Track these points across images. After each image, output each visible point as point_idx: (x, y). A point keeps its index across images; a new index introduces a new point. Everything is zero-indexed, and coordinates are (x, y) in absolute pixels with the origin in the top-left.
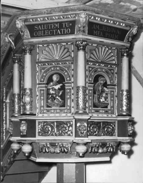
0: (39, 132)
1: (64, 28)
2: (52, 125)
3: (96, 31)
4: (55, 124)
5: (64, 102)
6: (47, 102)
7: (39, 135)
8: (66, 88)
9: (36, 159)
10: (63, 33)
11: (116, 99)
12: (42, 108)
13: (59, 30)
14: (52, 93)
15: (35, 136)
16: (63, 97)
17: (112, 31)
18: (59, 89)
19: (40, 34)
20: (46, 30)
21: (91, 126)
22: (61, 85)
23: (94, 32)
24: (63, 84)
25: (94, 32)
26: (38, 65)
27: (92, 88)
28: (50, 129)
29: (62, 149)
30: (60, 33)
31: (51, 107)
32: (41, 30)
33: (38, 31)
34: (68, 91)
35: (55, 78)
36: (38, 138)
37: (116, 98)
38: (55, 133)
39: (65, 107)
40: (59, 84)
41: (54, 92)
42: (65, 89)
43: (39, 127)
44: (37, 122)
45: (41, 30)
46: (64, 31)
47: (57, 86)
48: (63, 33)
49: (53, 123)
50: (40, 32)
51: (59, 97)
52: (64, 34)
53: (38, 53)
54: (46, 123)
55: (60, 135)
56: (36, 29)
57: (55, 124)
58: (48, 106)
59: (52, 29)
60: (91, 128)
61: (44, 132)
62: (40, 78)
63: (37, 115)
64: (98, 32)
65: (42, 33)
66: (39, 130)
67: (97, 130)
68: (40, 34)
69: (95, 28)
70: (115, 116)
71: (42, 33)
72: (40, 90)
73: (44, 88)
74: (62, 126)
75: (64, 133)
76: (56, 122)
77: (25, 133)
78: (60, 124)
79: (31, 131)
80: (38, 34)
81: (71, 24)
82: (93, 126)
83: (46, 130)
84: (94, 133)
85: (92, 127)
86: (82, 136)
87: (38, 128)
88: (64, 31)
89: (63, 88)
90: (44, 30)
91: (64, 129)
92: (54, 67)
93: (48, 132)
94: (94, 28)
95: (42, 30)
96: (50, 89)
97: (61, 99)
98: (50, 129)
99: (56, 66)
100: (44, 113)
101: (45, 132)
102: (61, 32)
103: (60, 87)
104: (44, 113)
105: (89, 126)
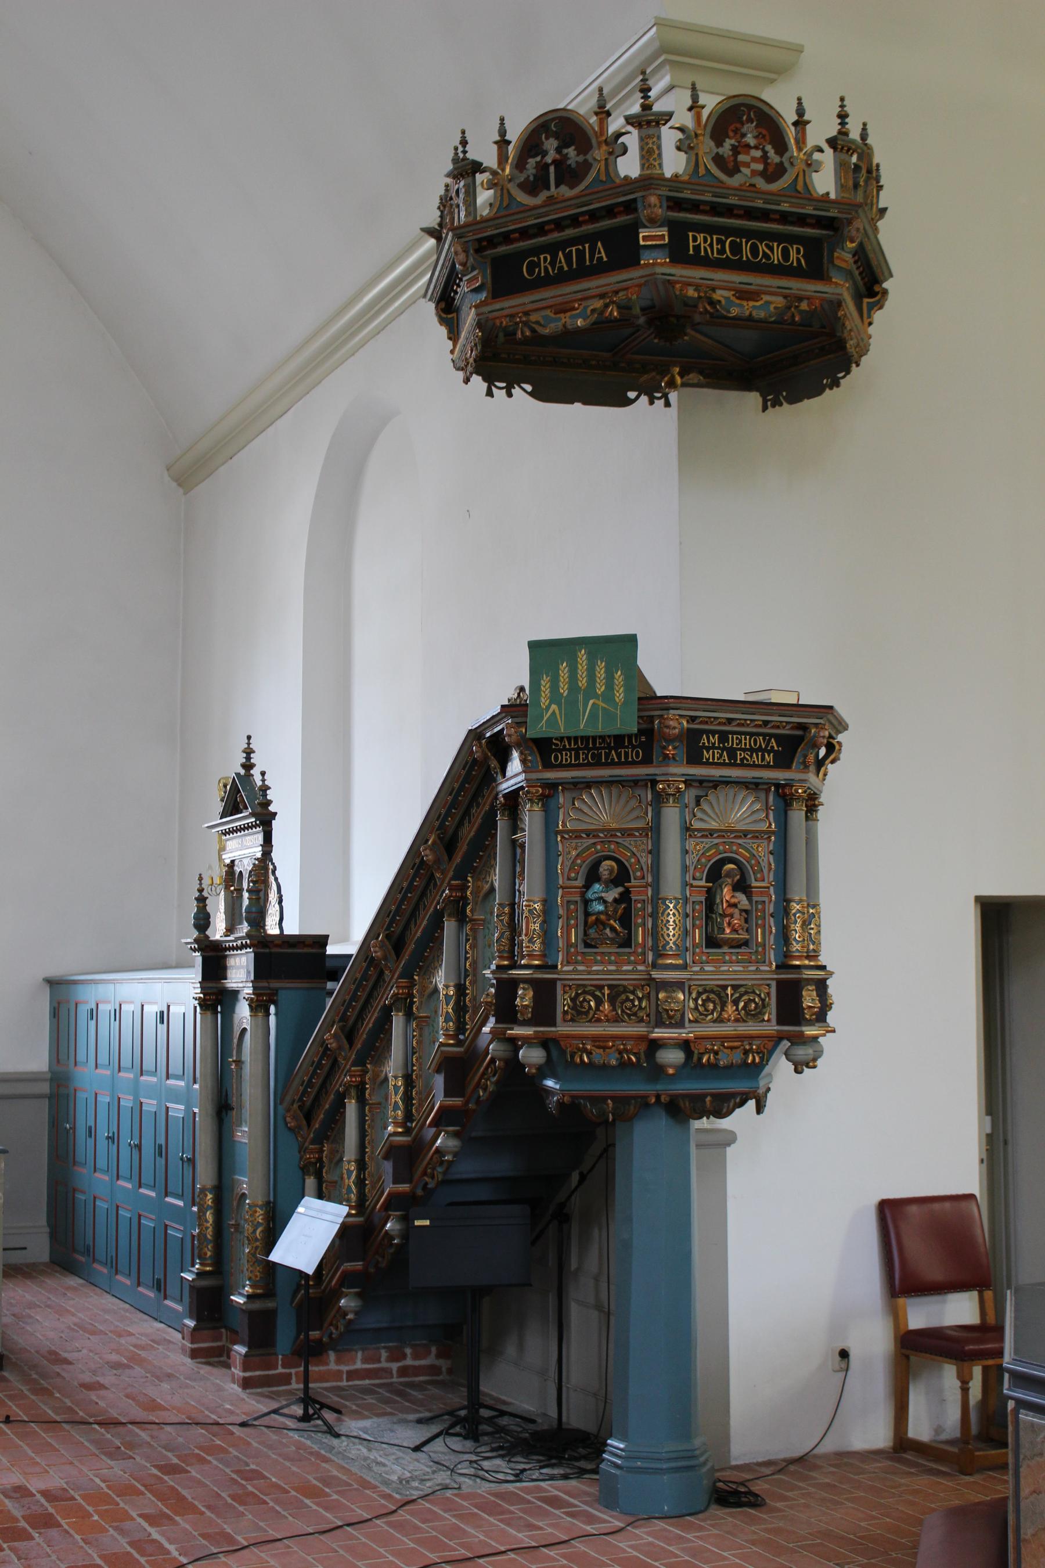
0: (565, 1013)
1: (627, 747)
2: (598, 993)
3: (711, 751)
4: (606, 991)
5: (630, 933)
6: (585, 934)
7: (565, 1021)
8: (633, 898)
9: (842, 195)
10: (623, 760)
11: (772, 924)
12: (572, 950)
13: (613, 752)
14: (683, 156)
15: (554, 1025)
16: (626, 920)
17: (755, 744)
18: (615, 900)
19: (566, 760)
20: (582, 749)
21: (699, 994)
22: (620, 889)
23: (705, 752)
24: (624, 887)
25: (705, 752)
26: (562, 837)
27: (703, 899)
28: (592, 1004)
29: (622, 1057)
30: (616, 760)
31: (595, 947)
32: (570, 750)
33: (560, 751)
34: (639, 905)
35: (607, 867)
36: (563, 1029)
37: (772, 920)
38: (606, 1016)
39: (631, 947)
40: (616, 886)
41: (601, 908)
42: (631, 899)
43: (564, 1000)
44: (559, 984)
45: (570, 750)
46: (626, 754)
47: (610, 892)
48: (623, 760)
49: (600, 988)
50: (566, 755)
51: (615, 921)
52: (627, 764)
53: (563, 806)
54: (584, 989)
55: (617, 1020)
56: (557, 745)
57: (606, 991)
58: (587, 945)
59: (598, 749)
60: (700, 1002)
61: (578, 1012)
62: (567, 870)
63: (559, 967)
64: (716, 751)
65: (571, 757)
66: (564, 1006)
67: (715, 1008)
68: (566, 760)
69: (707, 744)
70: (767, 968)
71: (571, 757)
72: (568, 902)
73: (609, 1461)
74: (623, 997)
75: (629, 1016)
76: (610, 987)
77: (530, 1015)
78: (617, 993)
79: (543, 1012)
80: (562, 760)
81: (643, 739)
82: (704, 997)
83: (582, 1007)
84: (706, 1016)
85: (703, 1000)
86: (671, 1023)
87: (563, 1002)
88: (626, 754)
89: (625, 897)
90: (577, 751)
91: (629, 1004)
92: (602, 842)
93: (587, 1013)
94: (704, 743)
95: (573, 749)
96: (592, 901)
97: (622, 925)
98: (592, 1004)
99: (609, 841)
100: (576, 962)
101: (579, 1013)
102: (619, 755)
103: (617, 896)
104: (567, 918)
105: (694, 995)
